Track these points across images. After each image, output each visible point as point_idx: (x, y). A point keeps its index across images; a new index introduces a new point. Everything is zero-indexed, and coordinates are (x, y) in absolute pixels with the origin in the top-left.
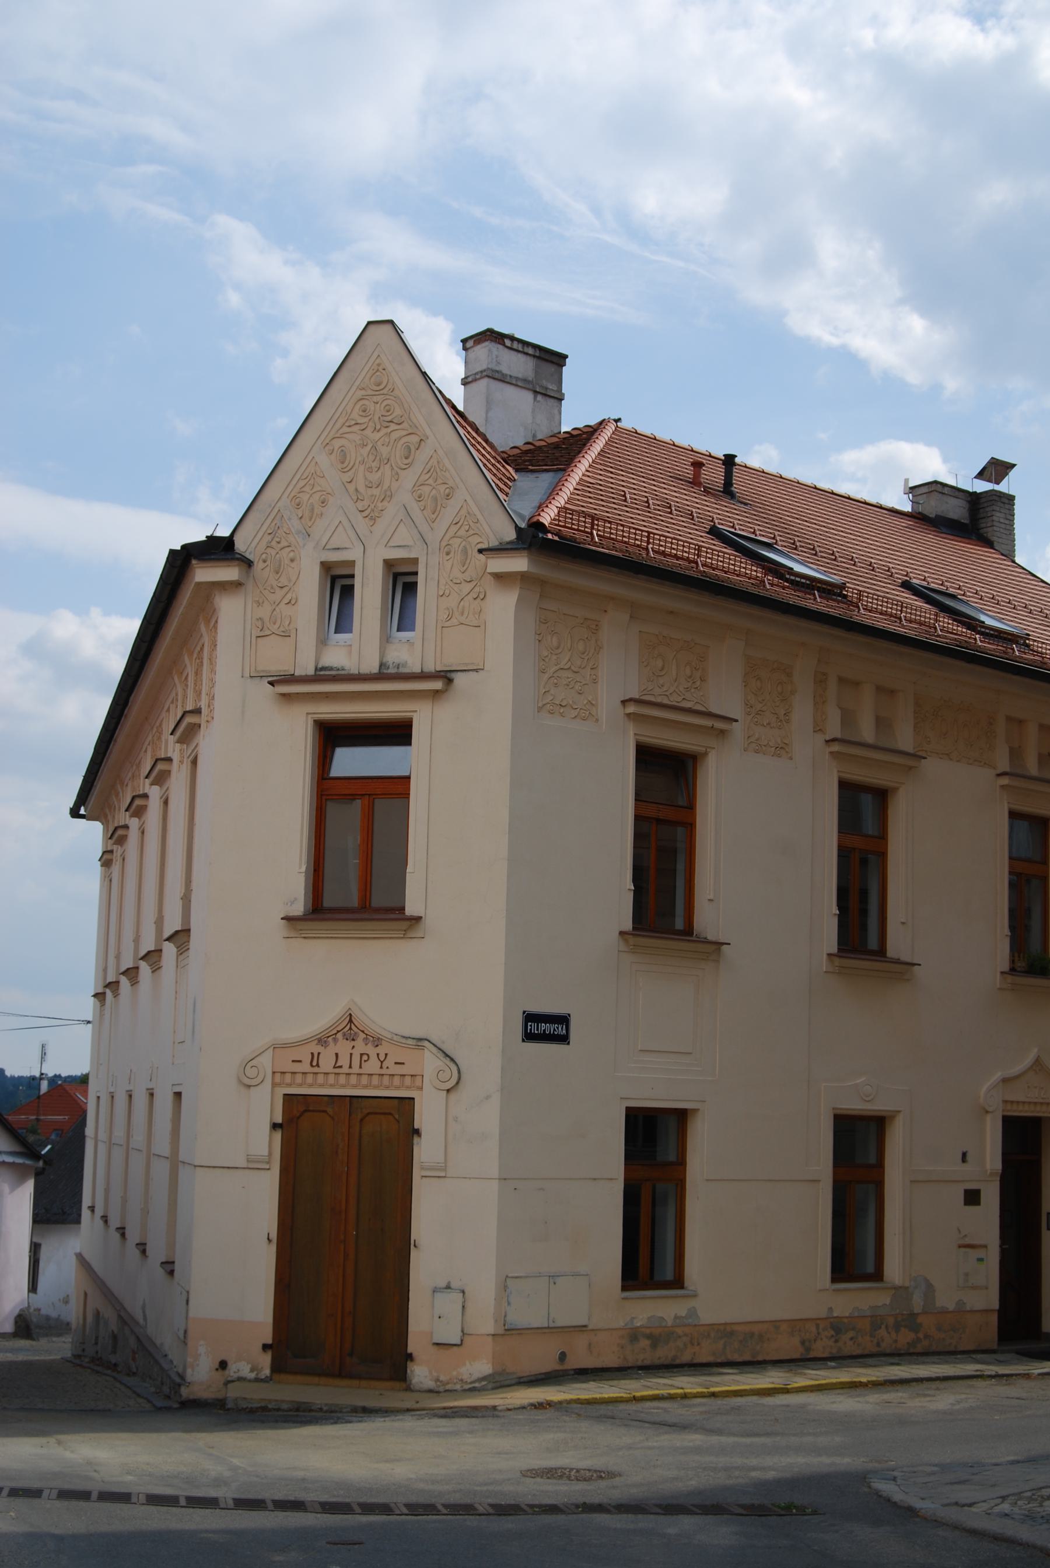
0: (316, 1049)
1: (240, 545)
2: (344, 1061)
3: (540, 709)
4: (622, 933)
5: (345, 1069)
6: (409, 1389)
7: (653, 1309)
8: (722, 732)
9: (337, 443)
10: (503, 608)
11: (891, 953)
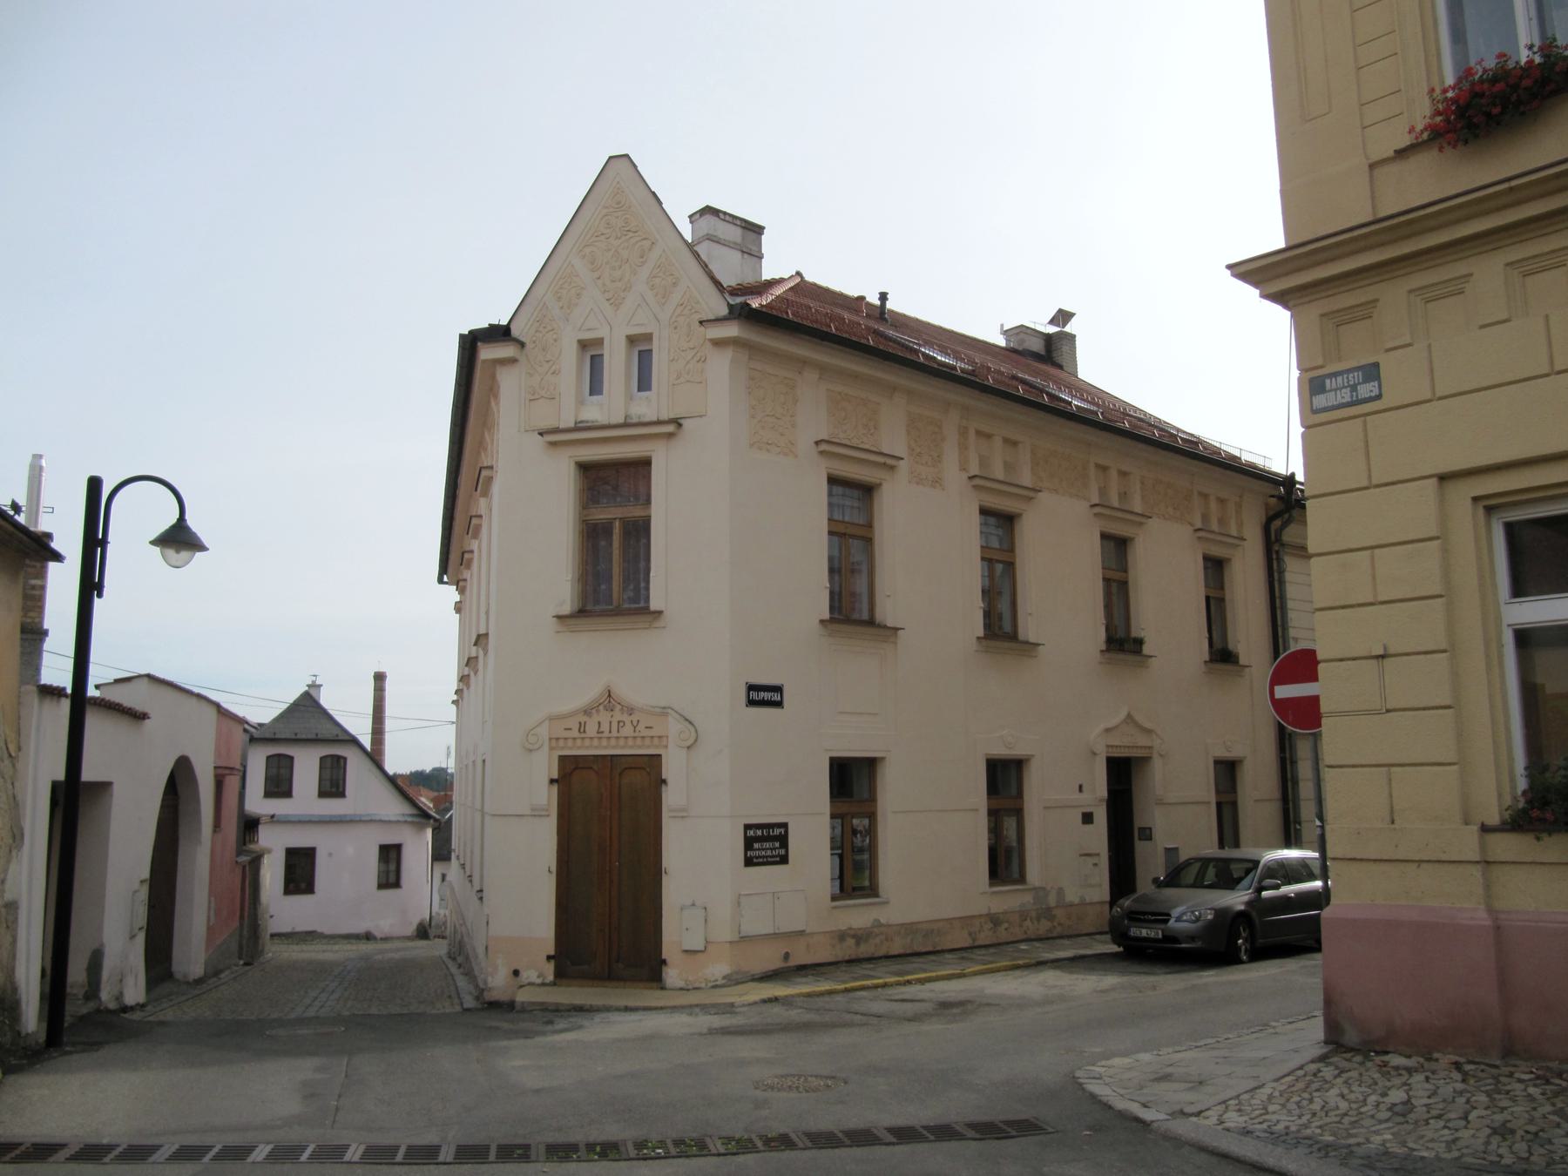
0: (583, 719)
1: (515, 332)
2: (605, 727)
3: (752, 445)
4: (822, 621)
5: (606, 734)
6: (663, 988)
7: (858, 915)
8: (892, 468)
9: (588, 250)
10: (721, 366)
11: (1021, 636)
